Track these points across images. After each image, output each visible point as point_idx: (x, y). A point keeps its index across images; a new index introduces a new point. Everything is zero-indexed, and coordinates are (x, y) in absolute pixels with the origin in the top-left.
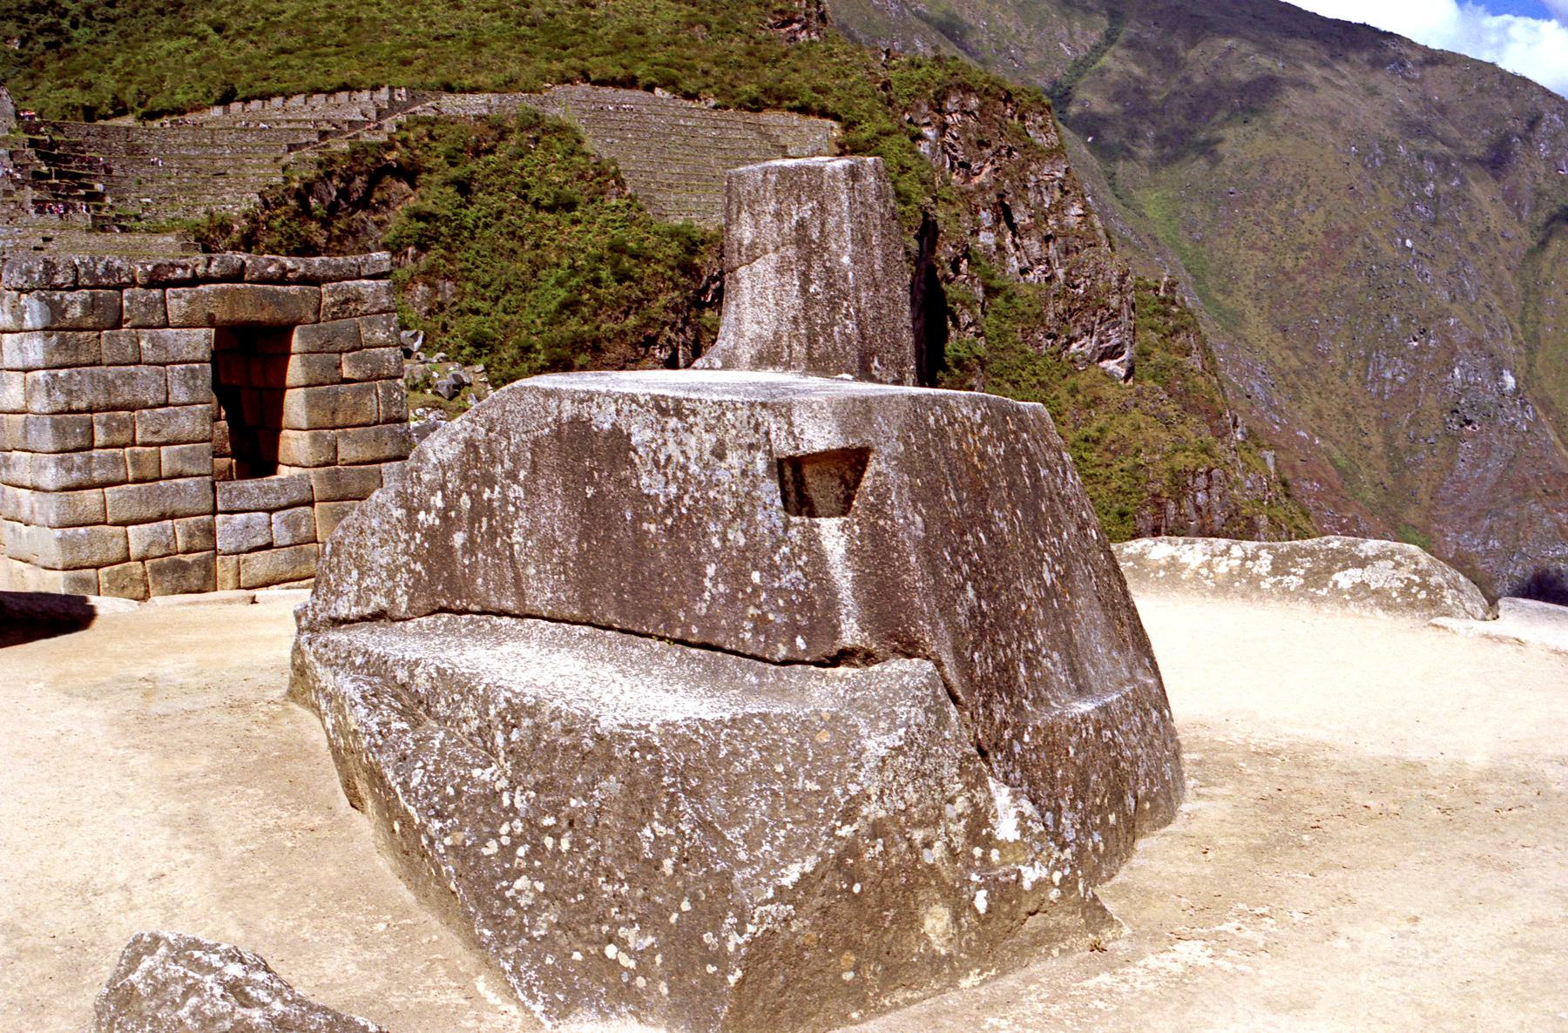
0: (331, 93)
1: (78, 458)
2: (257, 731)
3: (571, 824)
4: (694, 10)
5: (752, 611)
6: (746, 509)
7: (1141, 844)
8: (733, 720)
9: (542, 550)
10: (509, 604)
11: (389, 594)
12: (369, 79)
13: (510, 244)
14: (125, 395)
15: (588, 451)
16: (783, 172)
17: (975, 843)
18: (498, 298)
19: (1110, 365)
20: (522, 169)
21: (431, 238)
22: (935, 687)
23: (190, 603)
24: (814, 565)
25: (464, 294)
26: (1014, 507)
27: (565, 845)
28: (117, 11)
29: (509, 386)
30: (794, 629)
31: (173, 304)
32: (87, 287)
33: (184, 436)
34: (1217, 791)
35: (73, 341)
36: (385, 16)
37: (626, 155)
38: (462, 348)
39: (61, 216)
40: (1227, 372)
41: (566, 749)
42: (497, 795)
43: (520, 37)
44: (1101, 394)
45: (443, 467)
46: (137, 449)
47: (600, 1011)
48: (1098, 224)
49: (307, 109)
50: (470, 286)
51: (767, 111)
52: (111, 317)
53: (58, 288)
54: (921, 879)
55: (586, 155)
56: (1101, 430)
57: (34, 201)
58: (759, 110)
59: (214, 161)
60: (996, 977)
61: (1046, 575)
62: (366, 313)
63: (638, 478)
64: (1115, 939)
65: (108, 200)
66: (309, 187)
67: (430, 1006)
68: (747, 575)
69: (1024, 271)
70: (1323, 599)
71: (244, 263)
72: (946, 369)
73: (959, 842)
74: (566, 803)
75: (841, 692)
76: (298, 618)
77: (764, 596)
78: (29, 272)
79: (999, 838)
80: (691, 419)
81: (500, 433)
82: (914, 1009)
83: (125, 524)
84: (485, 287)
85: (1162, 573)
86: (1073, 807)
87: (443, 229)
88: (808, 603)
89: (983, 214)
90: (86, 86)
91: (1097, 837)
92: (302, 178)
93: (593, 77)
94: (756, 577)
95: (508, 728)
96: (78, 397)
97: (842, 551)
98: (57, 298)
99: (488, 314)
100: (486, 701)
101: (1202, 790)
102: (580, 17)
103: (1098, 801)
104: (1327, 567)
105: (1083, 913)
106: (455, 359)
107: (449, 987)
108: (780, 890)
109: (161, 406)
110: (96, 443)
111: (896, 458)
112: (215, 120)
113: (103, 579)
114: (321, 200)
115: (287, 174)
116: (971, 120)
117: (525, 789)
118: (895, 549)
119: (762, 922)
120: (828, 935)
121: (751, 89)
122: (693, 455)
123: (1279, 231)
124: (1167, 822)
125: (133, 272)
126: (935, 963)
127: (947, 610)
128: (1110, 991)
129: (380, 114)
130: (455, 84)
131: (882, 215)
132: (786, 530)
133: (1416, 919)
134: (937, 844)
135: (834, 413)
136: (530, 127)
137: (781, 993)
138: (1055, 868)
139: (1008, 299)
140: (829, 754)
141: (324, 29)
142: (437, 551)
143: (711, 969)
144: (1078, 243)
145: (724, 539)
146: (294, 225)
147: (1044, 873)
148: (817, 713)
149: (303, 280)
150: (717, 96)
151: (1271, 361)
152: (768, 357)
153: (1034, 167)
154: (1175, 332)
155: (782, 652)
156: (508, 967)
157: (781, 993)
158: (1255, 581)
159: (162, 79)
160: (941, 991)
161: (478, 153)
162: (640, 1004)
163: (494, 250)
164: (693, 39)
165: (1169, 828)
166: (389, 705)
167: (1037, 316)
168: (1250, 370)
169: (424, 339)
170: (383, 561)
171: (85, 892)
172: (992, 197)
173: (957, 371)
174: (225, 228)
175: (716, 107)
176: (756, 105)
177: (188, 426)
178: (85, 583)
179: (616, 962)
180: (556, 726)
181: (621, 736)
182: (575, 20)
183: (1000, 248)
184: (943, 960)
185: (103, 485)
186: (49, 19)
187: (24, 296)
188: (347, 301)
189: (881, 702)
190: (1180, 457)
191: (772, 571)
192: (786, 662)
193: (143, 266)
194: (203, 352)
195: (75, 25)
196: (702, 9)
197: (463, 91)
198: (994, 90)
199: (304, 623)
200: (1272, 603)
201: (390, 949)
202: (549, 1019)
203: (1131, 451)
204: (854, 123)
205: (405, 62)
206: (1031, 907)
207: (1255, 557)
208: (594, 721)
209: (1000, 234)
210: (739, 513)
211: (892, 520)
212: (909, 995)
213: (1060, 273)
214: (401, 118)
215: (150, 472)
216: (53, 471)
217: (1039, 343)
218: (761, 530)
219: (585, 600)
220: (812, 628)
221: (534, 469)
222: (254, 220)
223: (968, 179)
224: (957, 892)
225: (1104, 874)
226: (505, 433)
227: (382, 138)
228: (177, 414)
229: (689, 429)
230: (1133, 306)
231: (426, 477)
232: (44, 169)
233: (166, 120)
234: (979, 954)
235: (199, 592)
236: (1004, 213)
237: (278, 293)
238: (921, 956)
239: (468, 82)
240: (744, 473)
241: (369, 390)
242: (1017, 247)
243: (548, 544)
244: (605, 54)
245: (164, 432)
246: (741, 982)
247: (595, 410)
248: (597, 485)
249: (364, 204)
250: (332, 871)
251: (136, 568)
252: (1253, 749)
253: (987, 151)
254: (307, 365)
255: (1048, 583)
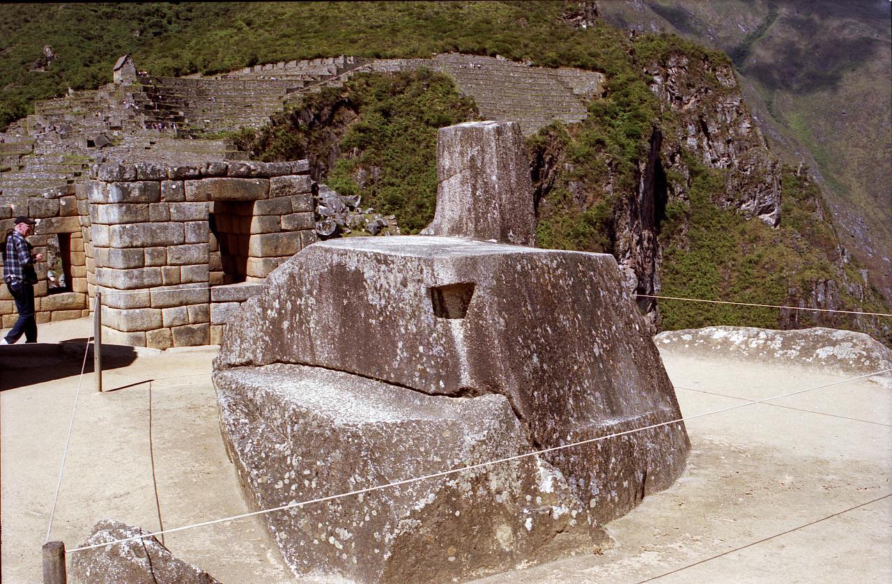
0: (311, 59)
1: (136, 272)
2: (198, 421)
3: (317, 474)
4: (520, 9)
5: (419, 366)
6: (417, 313)
7: (647, 499)
8: (402, 423)
9: (324, 332)
10: (308, 359)
11: (254, 352)
12: (333, 51)
13: (412, 146)
14: (162, 238)
15: (344, 281)
16: (464, 130)
17: (527, 493)
18: (405, 177)
19: (766, 217)
20: (419, 102)
21: (367, 142)
22: (506, 409)
23: (188, 352)
24: (448, 344)
25: (385, 174)
26: (576, 312)
27: (314, 485)
28: (193, 14)
29: (309, 246)
30: (439, 377)
31: (188, 189)
32: (142, 180)
33: (193, 261)
34: (702, 471)
35: (134, 209)
36: (342, 15)
37: (479, 94)
38: (384, 205)
39: (160, 130)
40: (841, 222)
41: (317, 435)
42: (285, 458)
43: (419, 26)
44: (760, 234)
45: (279, 287)
46: (168, 267)
47: (324, 570)
48: (759, 133)
49: (298, 68)
50: (389, 170)
51: (562, 68)
52: (155, 195)
53: (126, 180)
54: (494, 511)
55: (456, 94)
56: (759, 256)
57: (146, 122)
58: (557, 67)
59: (245, 98)
60: (537, 565)
61: (596, 350)
62: (295, 193)
63: (367, 295)
64: (610, 549)
65: (186, 121)
66: (298, 113)
67: (240, 564)
68: (417, 348)
69: (714, 161)
70: (810, 364)
71: (227, 166)
72: (666, 219)
73: (517, 492)
74: (315, 463)
75: (459, 411)
76: (213, 363)
77: (425, 359)
78: (111, 172)
79: (541, 491)
80: (392, 266)
81: (305, 270)
82: (488, 579)
83: (161, 308)
84: (397, 170)
85: (719, 347)
86: (598, 477)
87: (374, 137)
88: (445, 364)
89: (690, 127)
90: (176, 57)
91: (614, 493)
92: (294, 108)
93: (461, 49)
94: (421, 349)
95: (293, 423)
96: (136, 239)
97: (462, 336)
98: (126, 186)
99: (399, 186)
100: (285, 409)
101: (695, 471)
102: (454, 14)
103: (616, 474)
104: (814, 345)
105: (591, 534)
106: (380, 212)
107: (253, 555)
108: (414, 512)
109: (181, 244)
110: (146, 264)
111: (490, 288)
112: (246, 75)
113: (148, 337)
114: (305, 121)
115: (286, 106)
116: (683, 72)
117: (298, 455)
118: (488, 336)
119: (403, 528)
120: (441, 537)
121: (552, 54)
122: (392, 284)
123: (873, 136)
124: (665, 488)
125: (167, 172)
126: (502, 555)
127: (517, 368)
128: (596, 575)
129: (339, 71)
130: (381, 54)
131: (516, 153)
132: (435, 325)
133: (783, 547)
134: (505, 492)
135: (453, 265)
136: (424, 78)
137: (413, 566)
138: (573, 508)
139: (704, 178)
140: (448, 442)
141: (307, 23)
142: (275, 331)
143: (377, 551)
144: (747, 144)
145: (406, 329)
146: (289, 135)
147: (567, 511)
148: (445, 421)
149: (260, 176)
150: (532, 59)
151: (867, 215)
152: (456, 230)
153: (721, 99)
154: (807, 197)
155: (433, 388)
156: (281, 546)
157: (413, 566)
158: (771, 352)
159: (217, 52)
160: (505, 571)
161: (394, 94)
162: (344, 568)
163: (403, 149)
164: (518, 26)
165: (666, 491)
166: (241, 410)
167: (722, 188)
168: (854, 221)
169: (362, 200)
170: (251, 335)
171: (90, 500)
172: (695, 117)
173: (672, 220)
174: (250, 136)
175: (531, 66)
176: (555, 65)
177: (196, 255)
178: (139, 339)
179: (334, 545)
180: (315, 423)
181: (344, 429)
182: (451, 16)
183: (700, 147)
184: (507, 554)
185: (149, 287)
186: (154, 19)
187: (109, 185)
188: (285, 187)
189: (477, 417)
190: (808, 273)
191: (429, 346)
192: (435, 394)
193: (172, 168)
194: (204, 215)
195: (170, 22)
196: (524, 9)
197: (386, 58)
198: (697, 53)
199: (215, 366)
200: (780, 366)
201: (230, 535)
202: (298, 573)
203: (778, 269)
204: (613, 74)
205: (353, 42)
206: (558, 528)
207: (773, 339)
208: (332, 421)
209: (700, 139)
210: (413, 315)
211: (486, 321)
212: (486, 571)
213: (736, 162)
214: (351, 73)
215: (175, 280)
216: (123, 278)
217: (722, 204)
218: (423, 325)
219: (343, 358)
220: (447, 376)
221: (320, 290)
222: (267, 132)
223: (681, 106)
224: (516, 518)
225: (617, 514)
226: (307, 270)
227: (340, 85)
228: (190, 248)
229: (390, 271)
230: (780, 182)
231: (271, 292)
232: (151, 103)
233: (219, 76)
234: (527, 551)
235: (201, 345)
236: (703, 127)
237: (246, 183)
238: (495, 552)
239: (389, 53)
240: (415, 295)
241: (296, 236)
242: (710, 147)
243: (326, 328)
244: (467, 35)
245: (182, 258)
246: (391, 558)
247: (348, 260)
248: (348, 299)
249: (329, 122)
250: (212, 494)
251: (166, 332)
252: (732, 449)
253: (693, 90)
254: (261, 221)
255: (597, 354)
